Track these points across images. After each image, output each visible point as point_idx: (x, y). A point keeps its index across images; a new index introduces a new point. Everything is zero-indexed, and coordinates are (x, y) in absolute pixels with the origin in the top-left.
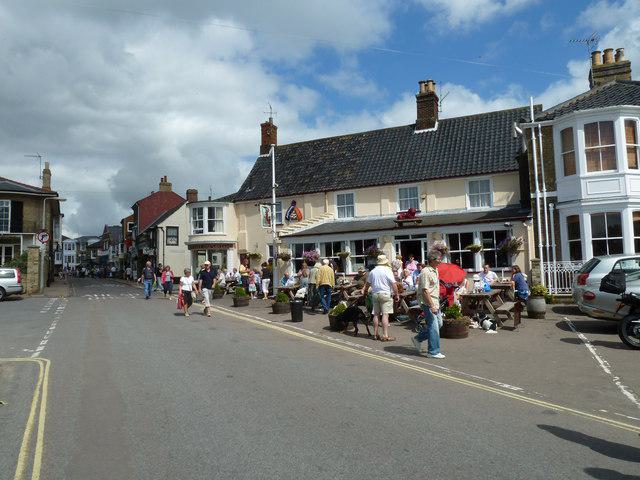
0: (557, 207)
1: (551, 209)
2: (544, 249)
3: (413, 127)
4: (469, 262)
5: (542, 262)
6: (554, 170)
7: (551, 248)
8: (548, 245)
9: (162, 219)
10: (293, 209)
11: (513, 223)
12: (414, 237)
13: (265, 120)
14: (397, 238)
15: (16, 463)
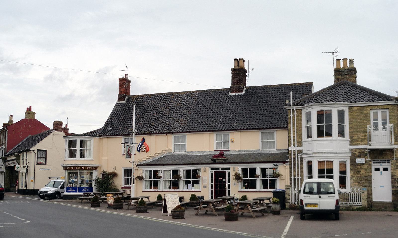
0: (303, 156)
1: (299, 157)
2: (295, 179)
3: (227, 90)
4: (253, 185)
6: (302, 134)
7: (298, 179)
8: (296, 177)
9: (34, 143)
10: (142, 144)
11: (277, 164)
12: (222, 169)
13: (122, 76)
14: (212, 169)
15: (350, 124)
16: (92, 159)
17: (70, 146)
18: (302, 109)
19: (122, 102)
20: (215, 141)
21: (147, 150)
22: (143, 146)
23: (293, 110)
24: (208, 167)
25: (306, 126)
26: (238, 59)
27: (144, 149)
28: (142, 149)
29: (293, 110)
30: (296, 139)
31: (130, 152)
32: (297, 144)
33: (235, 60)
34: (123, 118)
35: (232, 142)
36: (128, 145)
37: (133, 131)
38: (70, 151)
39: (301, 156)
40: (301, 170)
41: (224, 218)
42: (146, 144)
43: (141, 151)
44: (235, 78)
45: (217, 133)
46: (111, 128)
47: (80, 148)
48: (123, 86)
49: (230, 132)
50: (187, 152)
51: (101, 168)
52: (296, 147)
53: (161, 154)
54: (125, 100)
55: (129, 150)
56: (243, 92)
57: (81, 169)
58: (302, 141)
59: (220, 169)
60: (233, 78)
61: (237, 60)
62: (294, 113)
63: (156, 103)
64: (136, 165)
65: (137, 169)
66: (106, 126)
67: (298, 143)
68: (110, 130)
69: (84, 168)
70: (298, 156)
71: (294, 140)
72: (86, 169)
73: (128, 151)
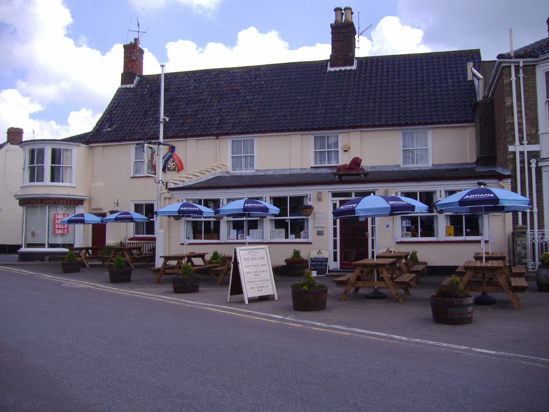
0: (540, 164)
1: (533, 166)
5: (529, 230)
7: (532, 214)
10: (171, 157)
14: (335, 195)
16: (74, 185)
17: (32, 161)
18: (534, 66)
19: (128, 86)
20: (312, 149)
21: (179, 168)
22: (172, 159)
23: (517, 68)
24: (326, 191)
25: (547, 101)
26: (343, 9)
27: (174, 165)
28: (169, 167)
29: (515, 66)
30: (526, 128)
31: (155, 162)
32: (527, 138)
33: (337, 10)
34: (133, 112)
35: (346, 151)
36: (150, 148)
37: (161, 120)
38: (32, 170)
39: (537, 164)
40: (537, 194)
41: (431, 313)
42: (176, 156)
43: (166, 170)
44: (338, 41)
45: (316, 134)
46: (109, 129)
47: (52, 164)
48: (131, 58)
49: (342, 132)
50: (257, 170)
51: (90, 201)
52: (525, 145)
53: (210, 172)
54: (135, 82)
55: (152, 158)
56: (355, 64)
57: (52, 203)
58: (539, 133)
59: (353, 195)
60: (335, 41)
61: (340, 9)
62: (519, 74)
63: (191, 86)
64: (166, 188)
65: (169, 198)
66: (100, 125)
67: (529, 138)
68: (107, 132)
69: (59, 202)
70: (529, 164)
71: (521, 131)
72: (62, 203)
73: (151, 160)
